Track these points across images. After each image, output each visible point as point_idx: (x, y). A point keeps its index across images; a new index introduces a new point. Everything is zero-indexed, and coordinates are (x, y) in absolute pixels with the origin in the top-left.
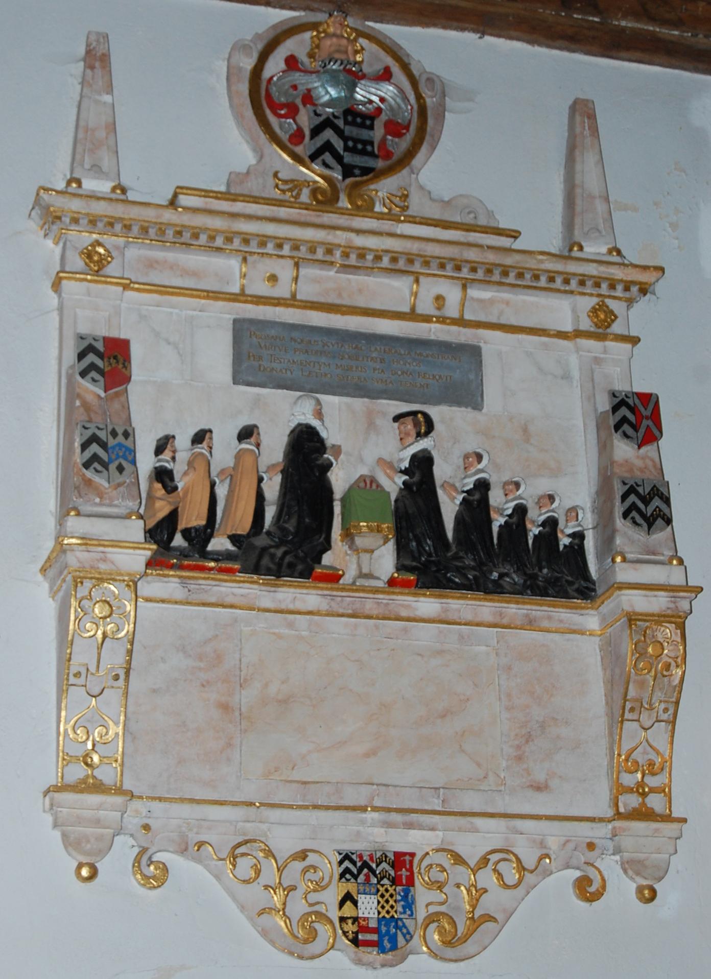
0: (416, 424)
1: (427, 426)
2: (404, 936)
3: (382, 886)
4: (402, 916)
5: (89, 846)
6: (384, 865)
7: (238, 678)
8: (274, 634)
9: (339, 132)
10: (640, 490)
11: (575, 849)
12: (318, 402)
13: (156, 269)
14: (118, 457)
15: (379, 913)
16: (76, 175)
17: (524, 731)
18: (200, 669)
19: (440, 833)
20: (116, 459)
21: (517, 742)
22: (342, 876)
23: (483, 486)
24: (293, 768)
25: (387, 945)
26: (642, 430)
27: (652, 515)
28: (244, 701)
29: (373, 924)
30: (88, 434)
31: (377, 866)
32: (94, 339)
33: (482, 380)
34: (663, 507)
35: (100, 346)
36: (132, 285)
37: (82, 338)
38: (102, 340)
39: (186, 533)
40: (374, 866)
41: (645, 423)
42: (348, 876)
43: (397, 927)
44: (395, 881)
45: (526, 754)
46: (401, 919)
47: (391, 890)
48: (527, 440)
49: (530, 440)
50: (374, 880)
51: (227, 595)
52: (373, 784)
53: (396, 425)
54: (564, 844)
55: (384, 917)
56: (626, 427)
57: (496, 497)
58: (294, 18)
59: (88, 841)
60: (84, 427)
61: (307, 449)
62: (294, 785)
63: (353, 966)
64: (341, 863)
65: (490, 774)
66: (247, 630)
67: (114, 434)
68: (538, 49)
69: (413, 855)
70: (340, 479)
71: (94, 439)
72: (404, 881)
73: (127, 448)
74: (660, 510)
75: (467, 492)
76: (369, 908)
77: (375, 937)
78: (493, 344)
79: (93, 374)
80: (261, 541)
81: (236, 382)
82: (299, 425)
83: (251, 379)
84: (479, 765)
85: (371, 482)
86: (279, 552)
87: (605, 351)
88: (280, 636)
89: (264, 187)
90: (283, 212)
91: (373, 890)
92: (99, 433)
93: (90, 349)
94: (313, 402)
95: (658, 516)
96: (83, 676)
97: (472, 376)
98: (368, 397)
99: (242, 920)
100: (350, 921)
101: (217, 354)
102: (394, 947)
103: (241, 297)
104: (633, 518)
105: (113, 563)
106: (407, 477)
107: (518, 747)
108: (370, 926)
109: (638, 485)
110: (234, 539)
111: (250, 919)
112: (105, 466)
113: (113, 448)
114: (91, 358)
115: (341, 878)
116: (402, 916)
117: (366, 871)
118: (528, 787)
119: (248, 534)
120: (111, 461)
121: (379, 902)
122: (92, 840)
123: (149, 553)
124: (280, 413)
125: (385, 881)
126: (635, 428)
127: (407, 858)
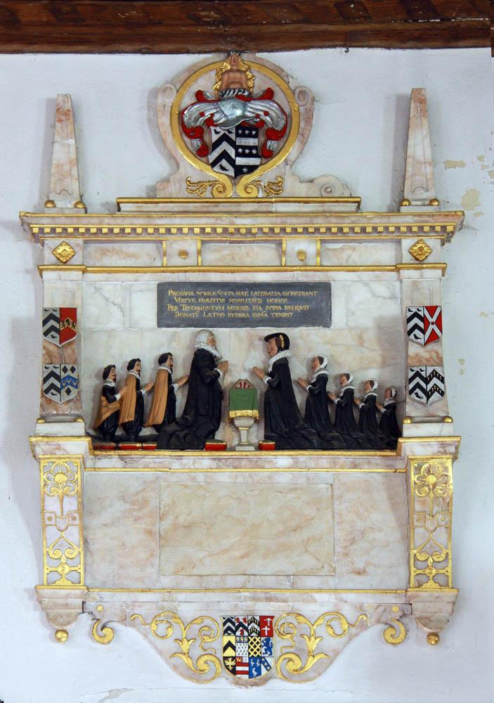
1: (284, 343)
2: (266, 667)
3: (252, 637)
4: (265, 655)
5: (62, 620)
6: (253, 624)
7: (158, 514)
8: (183, 485)
9: (232, 143)
10: (423, 374)
11: (384, 611)
12: (211, 334)
13: (107, 255)
14: (67, 384)
15: (249, 654)
16: (51, 199)
17: (350, 537)
18: (134, 510)
19: (291, 604)
20: (66, 386)
21: (345, 544)
22: (225, 632)
23: (323, 380)
24: (193, 568)
25: (255, 673)
27: (431, 390)
28: (162, 527)
29: (246, 660)
30: (49, 371)
31: (249, 625)
32: (54, 311)
33: (331, 307)
35: (57, 314)
36: (88, 269)
37: (45, 310)
38: (59, 311)
39: (124, 425)
40: (246, 625)
41: (431, 327)
42: (229, 632)
43: (261, 662)
44: (260, 634)
45: (351, 551)
46: (264, 657)
47: (258, 639)
48: (361, 345)
49: (347, 348)
50: (246, 633)
51: (150, 463)
52: (246, 575)
54: (376, 608)
55: (253, 656)
56: (417, 332)
57: (331, 387)
58: (207, 59)
59: (62, 617)
60: (46, 368)
61: (204, 364)
62: (195, 577)
63: (233, 686)
64: (224, 624)
65: (326, 565)
66: (163, 484)
67: (65, 370)
68: (393, 52)
69: (272, 617)
70: (226, 381)
71: (52, 374)
72: (266, 634)
73: (73, 378)
74: (437, 386)
75: (312, 384)
76: (242, 651)
77: (246, 669)
78: (339, 280)
79: (53, 333)
80: (172, 428)
81: (159, 325)
84: (318, 559)
85: (245, 383)
86: (182, 435)
87: (422, 277)
88: (186, 487)
89: (180, 189)
90: (191, 207)
91: (246, 640)
92: (55, 370)
93: (51, 317)
94: (207, 334)
95: (435, 391)
96: (54, 520)
97: (323, 305)
98: (250, 327)
99: (160, 660)
100: (230, 659)
101: (146, 307)
102: (259, 673)
103: (164, 269)
104: (417, 394)
105: (64, 450)
106: (270, 378)
107: (346, 547)
108: (244, 662)
109: (422, 371)
110: (156, 427)
111: (166, 661)
112: (59, 390)
113: (64, 379)
114: (52, 323)
115: (224, 634)
116: (265, 655)
117: (241, 628)
118: (352, 572)
119: (164, 422)
120: (62, 387)
121: (249, 647)
122: (64, 617)
124: (181, 343)
125: (254, 634)
127: (269, 619)
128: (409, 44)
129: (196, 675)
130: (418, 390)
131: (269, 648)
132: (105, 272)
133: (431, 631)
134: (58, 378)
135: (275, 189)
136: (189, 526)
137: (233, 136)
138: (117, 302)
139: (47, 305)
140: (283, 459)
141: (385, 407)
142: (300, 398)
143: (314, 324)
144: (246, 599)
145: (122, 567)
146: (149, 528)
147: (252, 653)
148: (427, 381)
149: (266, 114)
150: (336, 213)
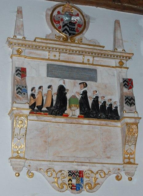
0: (84, 85)
5: (18, 169)
6: (77, 173)
9: (68, 26)
10: (129, 98)
12: (64, 80)
18: (40, 134)
22: (69, 175)
23: (97, 97)
25: (78, 189)
26: (129, 86)
29: (75, 185)
30: (18, 87)
34: (133, 101)
35: (20, 69)
39: (37, 107)
43: (80, 186)
44: (79, 176)
53: (80, 85)
56: (126, 85)
57: (100, 100)
61: (62, 90)
63: (71, 193)
64: (69, 173)
67: (23, 87)
69: (83, 171)
70: (68, 96)
73: (26, 90)
77: (75, 188)
78: (99, 69)
79: (19, 75)
80: (52, 108)
82: (60, 85)
83: (51, 76)
86: (56, 111)
90: (57, 42)
92: (20, 87)
98: (74, 79)
100: (70, 184)
101: (43, 71)
102: (79, 190)
103: (48, 59)
110: (47, 108)
114: (18, 72)
120: (22, 92)
123: (30, 111)
124: (56, 83)
125: (78, 176)
126: (128, 86)
127: (82, 172)
128: (112, 9)
129: (61, 188)
130: (127, 103)
131: (82, 181)
132: (31, 58)
133: (130, 177)
134: (21, 89)
135: (80, 42)
136: (57, 140)
137: (68, 25)
138: (34, 68)
139: (17, 66)
140: (86, 121)
141: (114, 107)
142: (90, 102)
143: (92, 81)
144: (75, 165)
145: (36, 152)
146: (45, 140)
147: (77, 183)
148: (130, 100)
149: (77, 20)
150: (98, 51)
